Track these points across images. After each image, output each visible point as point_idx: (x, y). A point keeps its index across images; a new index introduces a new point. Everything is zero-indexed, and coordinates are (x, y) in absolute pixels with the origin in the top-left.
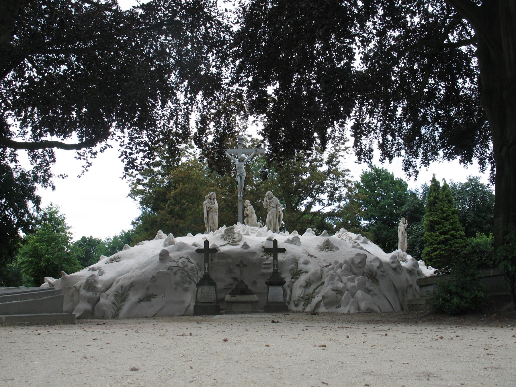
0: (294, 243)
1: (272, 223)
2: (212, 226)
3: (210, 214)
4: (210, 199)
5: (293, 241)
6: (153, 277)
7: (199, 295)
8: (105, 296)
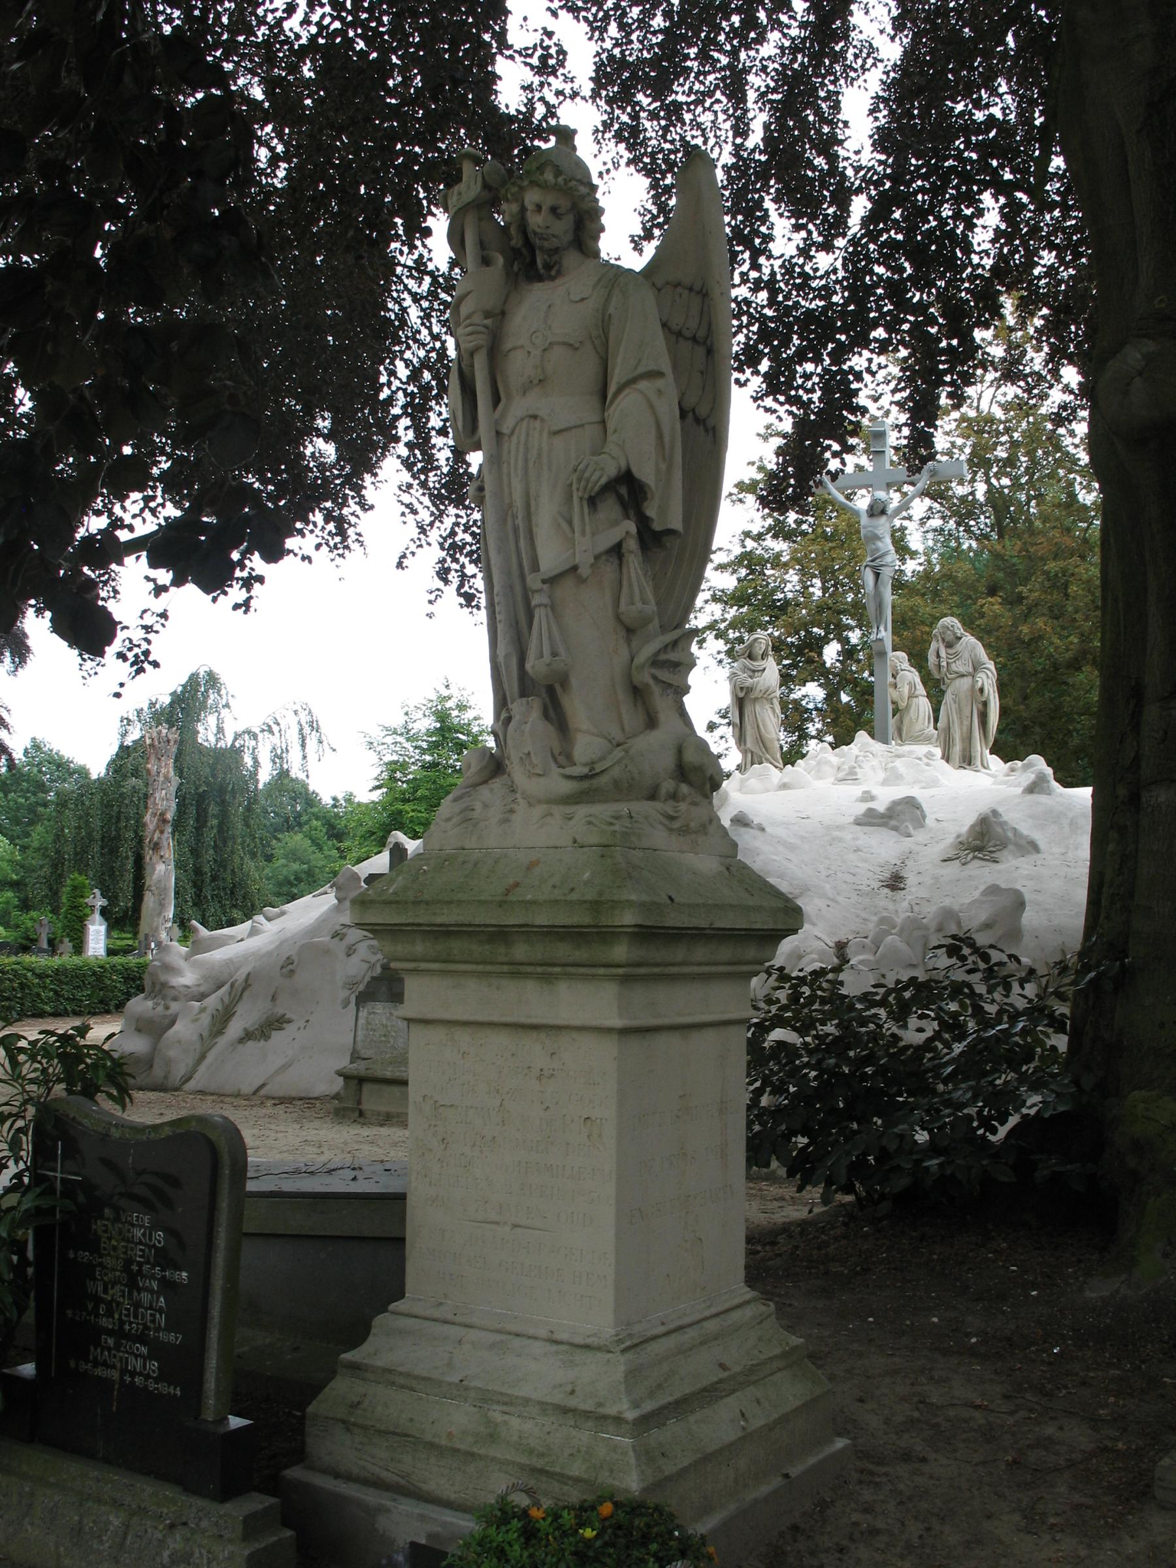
0: (893, 823)
1: (957, 735)
2: (756, 750)
3: (748, 710)
4: (751, 657)
5: (890, 817)
6: (289, 961)
7: (359, 1038)
8: (196, 1011)
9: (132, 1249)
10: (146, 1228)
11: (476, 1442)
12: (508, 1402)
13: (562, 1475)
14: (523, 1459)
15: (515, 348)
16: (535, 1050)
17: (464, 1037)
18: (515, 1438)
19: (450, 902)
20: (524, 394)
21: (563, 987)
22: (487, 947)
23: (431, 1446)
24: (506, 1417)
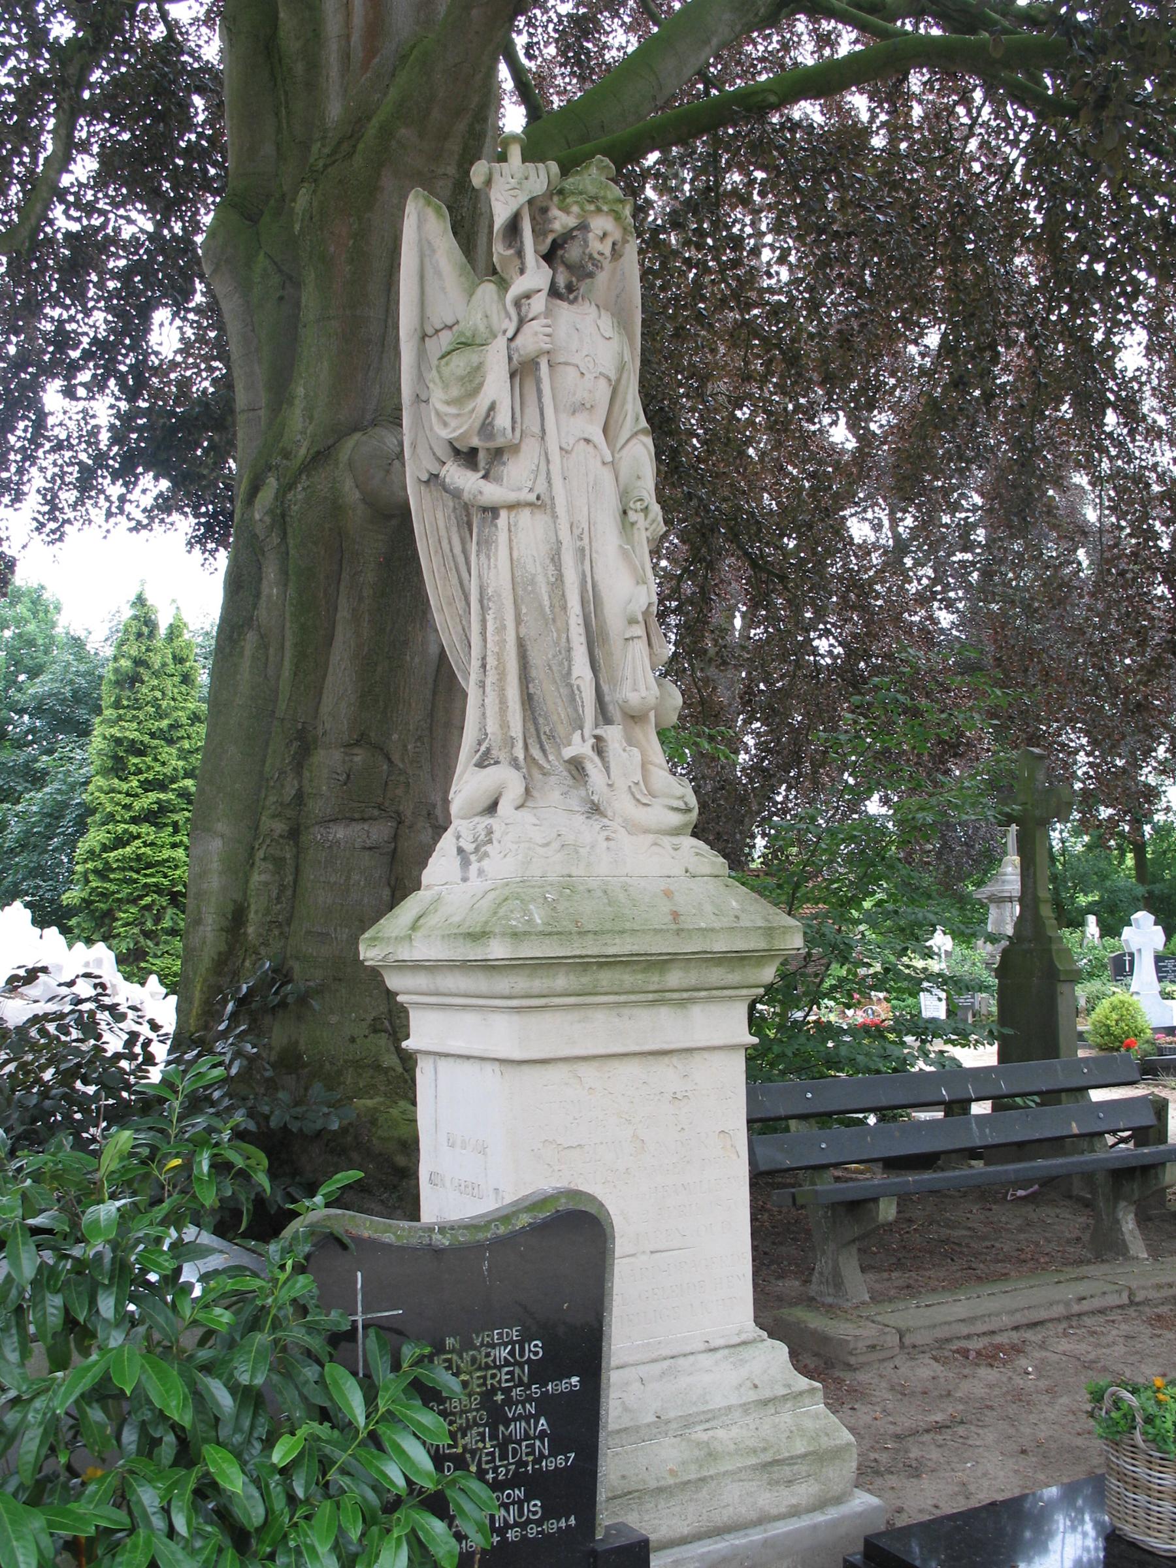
9: (493, 1376)
10: (513, 1343)
11: (701, 1467)
12: (710, 1418)
13: (792, 1458)
14: (753, 1461)
15: (566, 364)
16: (666, 1074)
17: (588, 1072)
18: (733, 1447)
19: (622, 932)
20: (574, 413)
21: (696, 1011)
22: (639, 976)
23: (660, 1490)
24: (710, 1433)
